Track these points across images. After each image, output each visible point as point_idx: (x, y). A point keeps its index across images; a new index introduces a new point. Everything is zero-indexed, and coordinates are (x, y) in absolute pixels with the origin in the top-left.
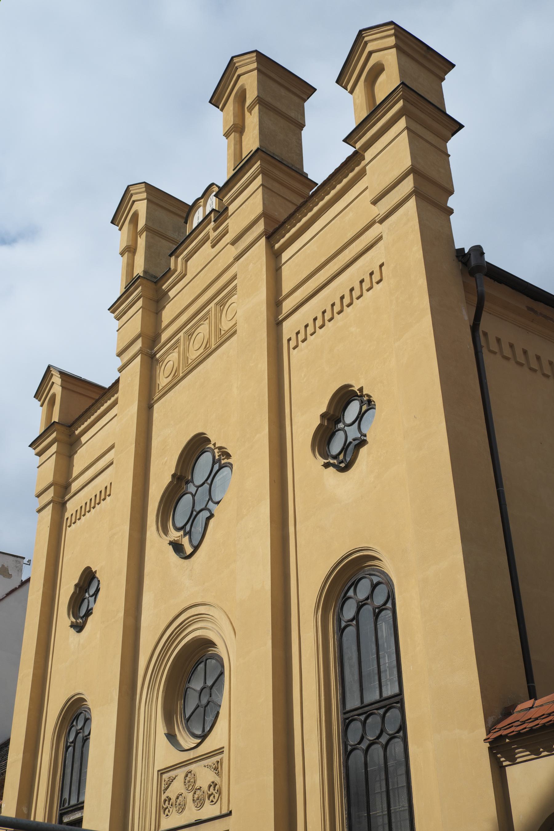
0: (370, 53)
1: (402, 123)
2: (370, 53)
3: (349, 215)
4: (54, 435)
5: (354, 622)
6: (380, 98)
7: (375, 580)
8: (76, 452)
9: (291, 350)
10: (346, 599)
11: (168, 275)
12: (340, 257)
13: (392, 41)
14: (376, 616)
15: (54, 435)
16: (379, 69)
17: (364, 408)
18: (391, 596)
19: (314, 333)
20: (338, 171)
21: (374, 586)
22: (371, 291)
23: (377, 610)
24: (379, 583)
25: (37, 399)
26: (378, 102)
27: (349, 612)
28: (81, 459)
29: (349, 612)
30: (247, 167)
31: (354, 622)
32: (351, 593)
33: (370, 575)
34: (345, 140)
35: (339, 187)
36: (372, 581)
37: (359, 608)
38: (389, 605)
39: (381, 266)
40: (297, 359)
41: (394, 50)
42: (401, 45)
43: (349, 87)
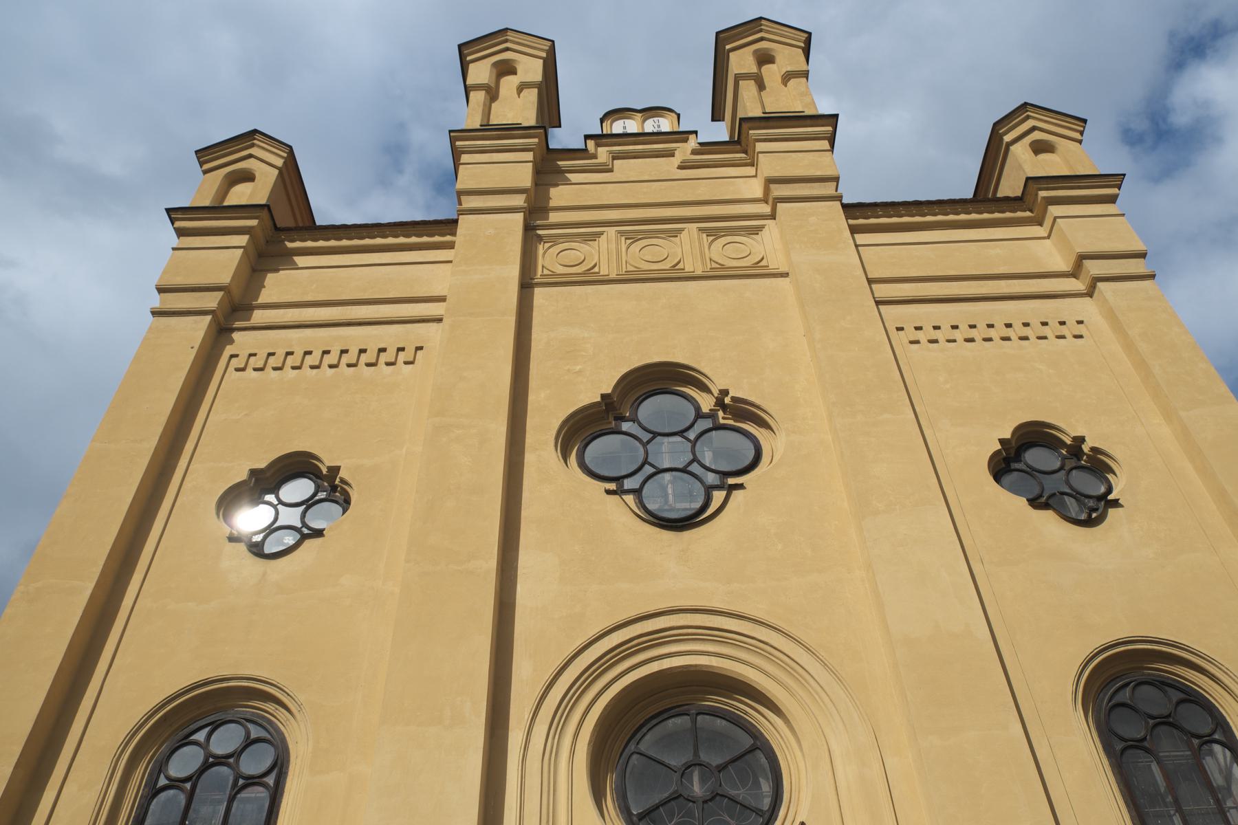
0: (250, 156)
1: (243, 240)
2: (250, 156)
3: (995, 250)
4: (253, 223)
5: (188, 786)
6: (231, 200)
7: (255, 732)
8: (277, 270)
9: (231, 369)
10: (185, 741)
11: (579, 155)
12: (1003, 283)
13: (279, 162)
14: (237, 790)
15: (254, 223)
16: (248, 177)
17: (322, 495)
18: (280, 766)
19: (243, 370)
20: (940, 203)
21: (249, 743)
22: (352, 369)
23: (241, 782)
24: (258, 740)
25: (198, 158)
26: (226, 204)
27: (184, 763)
28: (276, 286)
29: (184, 763)
30: (808, 122)
31: (188, 786)
32: (200, 736)
33: (248, 720)
34: (168, 211)
35: (974, 216)
36: (248, 733)
37: (206, 767)
38: (270, 780)
39: (419, 348)
40: (231, 386)
41: (276, 172)
42: (284, 171)
43: (206, 166)
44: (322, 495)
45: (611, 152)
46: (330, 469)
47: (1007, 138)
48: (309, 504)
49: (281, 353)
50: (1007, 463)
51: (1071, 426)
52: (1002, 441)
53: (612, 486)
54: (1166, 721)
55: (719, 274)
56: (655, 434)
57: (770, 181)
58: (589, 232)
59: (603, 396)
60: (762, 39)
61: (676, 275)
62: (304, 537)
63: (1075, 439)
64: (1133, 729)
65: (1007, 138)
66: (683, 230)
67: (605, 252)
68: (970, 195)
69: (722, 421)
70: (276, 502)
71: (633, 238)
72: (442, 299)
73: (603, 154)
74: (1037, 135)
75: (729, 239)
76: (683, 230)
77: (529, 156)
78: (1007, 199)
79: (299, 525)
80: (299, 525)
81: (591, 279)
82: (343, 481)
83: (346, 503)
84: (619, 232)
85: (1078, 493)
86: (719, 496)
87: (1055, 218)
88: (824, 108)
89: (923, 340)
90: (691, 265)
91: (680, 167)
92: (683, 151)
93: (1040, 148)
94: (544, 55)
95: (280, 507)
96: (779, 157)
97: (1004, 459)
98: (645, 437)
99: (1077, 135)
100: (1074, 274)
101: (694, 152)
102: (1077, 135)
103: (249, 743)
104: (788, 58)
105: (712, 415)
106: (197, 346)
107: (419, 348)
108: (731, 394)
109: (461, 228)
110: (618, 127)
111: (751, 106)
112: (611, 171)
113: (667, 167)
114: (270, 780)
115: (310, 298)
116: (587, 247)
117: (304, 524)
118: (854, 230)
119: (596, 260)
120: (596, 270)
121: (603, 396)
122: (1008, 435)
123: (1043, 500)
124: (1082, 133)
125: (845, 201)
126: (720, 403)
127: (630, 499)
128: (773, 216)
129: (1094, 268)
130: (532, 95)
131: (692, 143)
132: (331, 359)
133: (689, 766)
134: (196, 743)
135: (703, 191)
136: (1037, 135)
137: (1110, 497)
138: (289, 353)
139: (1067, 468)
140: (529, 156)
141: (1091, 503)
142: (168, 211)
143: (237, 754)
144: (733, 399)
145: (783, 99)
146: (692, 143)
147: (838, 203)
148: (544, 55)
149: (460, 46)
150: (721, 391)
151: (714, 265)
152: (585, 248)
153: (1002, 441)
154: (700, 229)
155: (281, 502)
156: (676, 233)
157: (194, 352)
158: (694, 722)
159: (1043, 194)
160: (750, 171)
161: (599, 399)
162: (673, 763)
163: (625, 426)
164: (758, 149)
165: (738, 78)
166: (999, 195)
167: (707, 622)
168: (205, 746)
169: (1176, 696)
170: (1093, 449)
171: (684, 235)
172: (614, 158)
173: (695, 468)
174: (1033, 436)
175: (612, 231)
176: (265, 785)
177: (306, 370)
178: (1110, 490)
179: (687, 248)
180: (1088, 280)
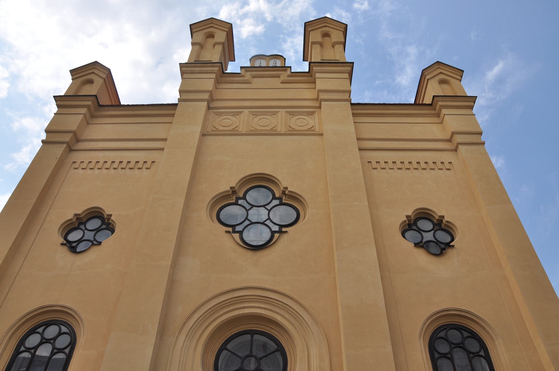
2: (93, 73)
4: (89, 103)
7: (64, 329)
9: (72, 168)
16: (91, 82)
17: (104, 227)
18: (72, 345)
21: (60, 334)
32: (40, 330)
34: (54, 97)
39: (153, 162)
42: (106, 79)
44: (104, 227)
45: (252, 75)
46: (108, 215)
47: (428, 77)
48: (98, 230)
49: (94, 161)
50: (410, 226)
51: (439, 211)
52: (407, 217)
53: (230, 229)
54: (461, 346)
55: (292, 133)
56: (253, 206)
57: (319, 91)
58: (236, 111)
59: (231, 188)
60: (326, 26)
61: (273, 133)
62: (93, 244)
63: (440, 216)
64: (443, 348)
65: (428, 77)
66: (279, 112)
67: (243, 121)
68: (412, 101)
69: (284, 201)
70: (84, 229)
71: (255, 115)
72: (165, 140)
73: (248, 76)
74: (442, 77)
75: (299, 117)
76: (279, 112)
77: (214, 76)
78: (425, 104)
79: (93, 240)
80: (93, 240)
81: (234, 133)
82: (112, 221)
83: (113, 231)
84: (250, 112)
85: (438, 241)
86: (277, 235)
87: (445, 115)
88: (348, 60)
89: (395, 167)
90: (281, 129)
91: (282, 83)
92: (284, 75)
93: (442, 82)
94: (227, 30)
95: (86, 231)
96: (326, 81)
97: (408, 224)
98: (248, 207)
99: (459, 78)
100: (450, 140)
101: (289, 76)
102: (459, 78)
103: (60, 334)
104: (336, 36)
105: (280, 199)
106: (58, 158)
107: (153, 162)
108: (289, 189)
109: (178, 108)
110: (257, 64)
111: (316, 58)
112: (250, 83)
113: (276, 82)
114: (67, 351)
115: (110, 137)
116: (235, 119)
117: (95, 240)
118: (354, 115)
119: (238, 124)
120: (237, 129)
121: (231, 188)
122: (410, 213)
123: (422, 244)
124: (461, 77)
125: (352, 102)
126: (284, 193)
127: (236, 236)
128: (320, 107)
129: (458, 139)
130: (219, 48)
131: (288, 72)
132: (99, 165)
133: (247, 356)
134: (38, 333)
135: (290, 94)
136: (442, 77)
137: (451, 244)
138: (98, 162)
139: (435, 229)
140: (214, 76)
141: (443, 246)
142: (54, 97)
143: (55, 339)
144: (289, 191)
145: (331, 55)
146: (288, 72)
147: (349, 103)
148: (227, 30)
149: (190, 25)
150: (284, 188)
151: (291, 129)
152: (234, 119)
153: (407, 217)
154: (287, 112)
155: (86, 229)
156: (275, 113)
157: (57, 160)
158: (252, 337)
159: (440, 103)
160: (312, 86)
161: (229, 189)
162: (240, 355)
163: (240, 202)
164: (318, 75)
165: (313, 43)
166: (424, 102)
167: (263, 294)
168: (42, 334)
169: (466, 334)
170: (447, 222)
171: (279, 114)
172: (253, 77)
173: (268, 222)
174: (423, 215)
175: (246, 111)
176: (65, 353)
177: (119, 170)
178: (453, 240)
179: (279, 120)
180: (455, 144)
